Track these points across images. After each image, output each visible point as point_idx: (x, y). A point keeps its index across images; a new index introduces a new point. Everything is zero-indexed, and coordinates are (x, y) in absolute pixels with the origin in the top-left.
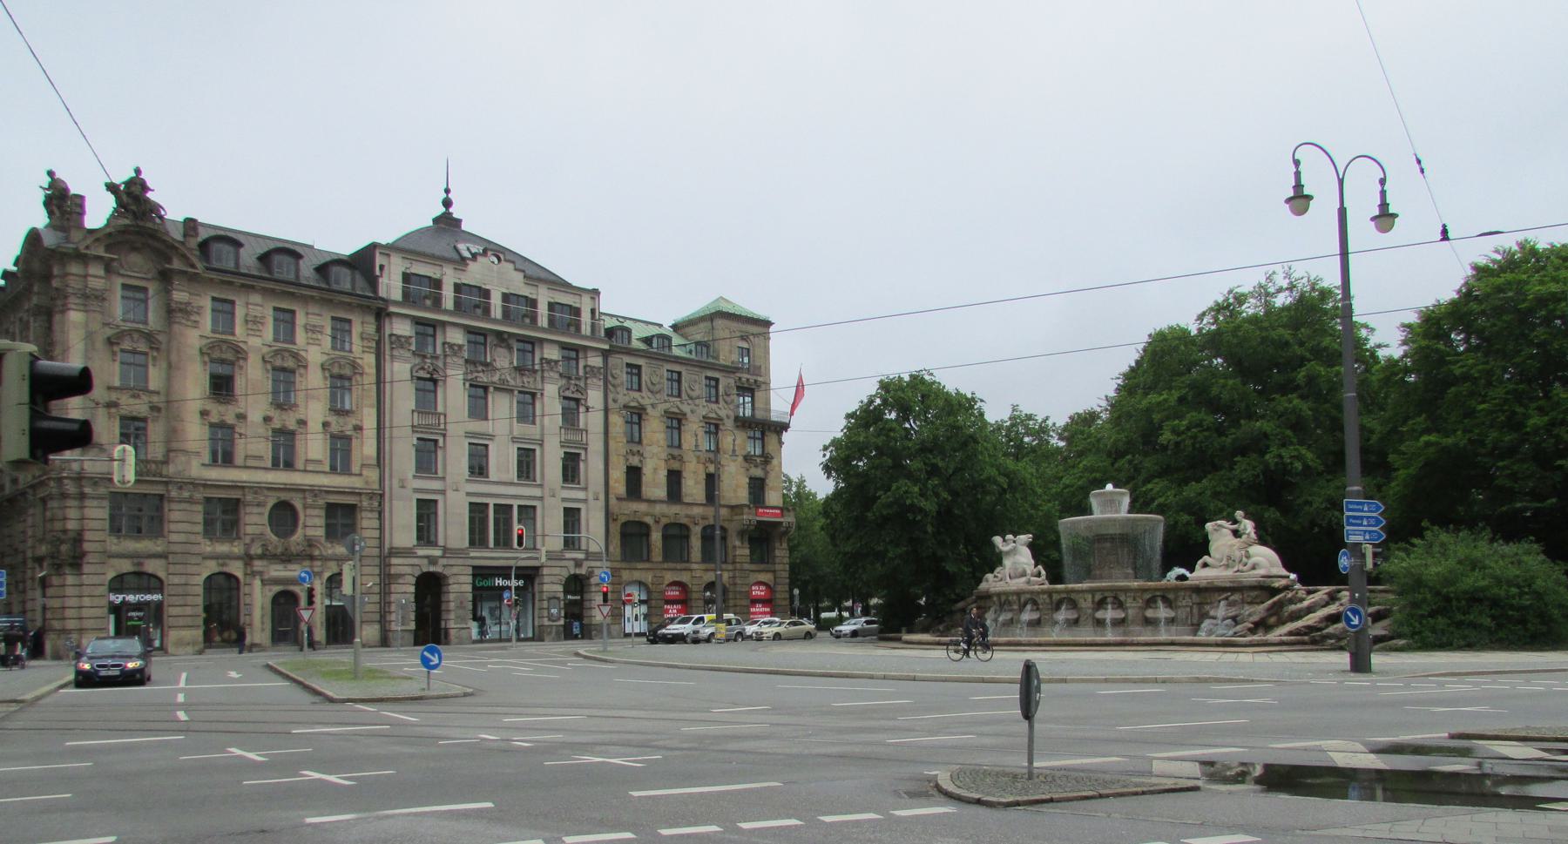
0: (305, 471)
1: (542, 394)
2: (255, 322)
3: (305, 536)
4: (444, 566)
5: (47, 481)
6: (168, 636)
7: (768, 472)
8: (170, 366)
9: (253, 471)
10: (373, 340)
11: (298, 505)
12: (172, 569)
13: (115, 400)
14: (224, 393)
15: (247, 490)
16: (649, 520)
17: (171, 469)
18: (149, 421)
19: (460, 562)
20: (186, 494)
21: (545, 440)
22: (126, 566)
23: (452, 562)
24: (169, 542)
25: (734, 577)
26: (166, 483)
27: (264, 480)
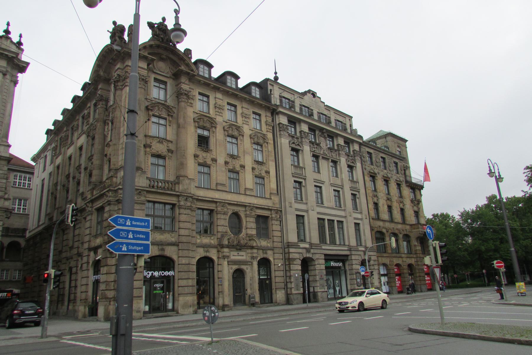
0: (245, 194)
1: (340, 162)
2: (220, 109)
3: (247, 234)
4: (313, 254)
5: (107, 193)
6: (178, 300)
7: (419, 208)
8: (179, 126)
9: (221, 192)
10: (272, 126)
11: (242, 215)
12: (181, 253)
13: (149, 143)
14: (203, 145)
15: (218, 204)
16: (384, 231)
17: (180, 188)
18: (167, 158)
19: (319, 251)
20: (189, 204)
21: (344, 186)
22: (154, 251)
23: (316, 251)
24: (179, 235)
25: (417, 261)
26: (178, 196)
27: (226, 198)
